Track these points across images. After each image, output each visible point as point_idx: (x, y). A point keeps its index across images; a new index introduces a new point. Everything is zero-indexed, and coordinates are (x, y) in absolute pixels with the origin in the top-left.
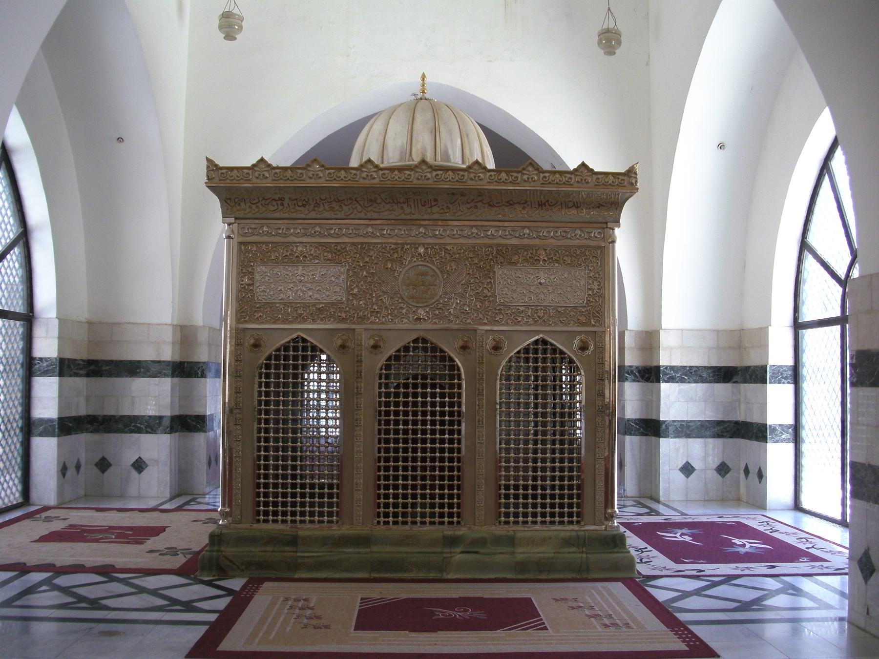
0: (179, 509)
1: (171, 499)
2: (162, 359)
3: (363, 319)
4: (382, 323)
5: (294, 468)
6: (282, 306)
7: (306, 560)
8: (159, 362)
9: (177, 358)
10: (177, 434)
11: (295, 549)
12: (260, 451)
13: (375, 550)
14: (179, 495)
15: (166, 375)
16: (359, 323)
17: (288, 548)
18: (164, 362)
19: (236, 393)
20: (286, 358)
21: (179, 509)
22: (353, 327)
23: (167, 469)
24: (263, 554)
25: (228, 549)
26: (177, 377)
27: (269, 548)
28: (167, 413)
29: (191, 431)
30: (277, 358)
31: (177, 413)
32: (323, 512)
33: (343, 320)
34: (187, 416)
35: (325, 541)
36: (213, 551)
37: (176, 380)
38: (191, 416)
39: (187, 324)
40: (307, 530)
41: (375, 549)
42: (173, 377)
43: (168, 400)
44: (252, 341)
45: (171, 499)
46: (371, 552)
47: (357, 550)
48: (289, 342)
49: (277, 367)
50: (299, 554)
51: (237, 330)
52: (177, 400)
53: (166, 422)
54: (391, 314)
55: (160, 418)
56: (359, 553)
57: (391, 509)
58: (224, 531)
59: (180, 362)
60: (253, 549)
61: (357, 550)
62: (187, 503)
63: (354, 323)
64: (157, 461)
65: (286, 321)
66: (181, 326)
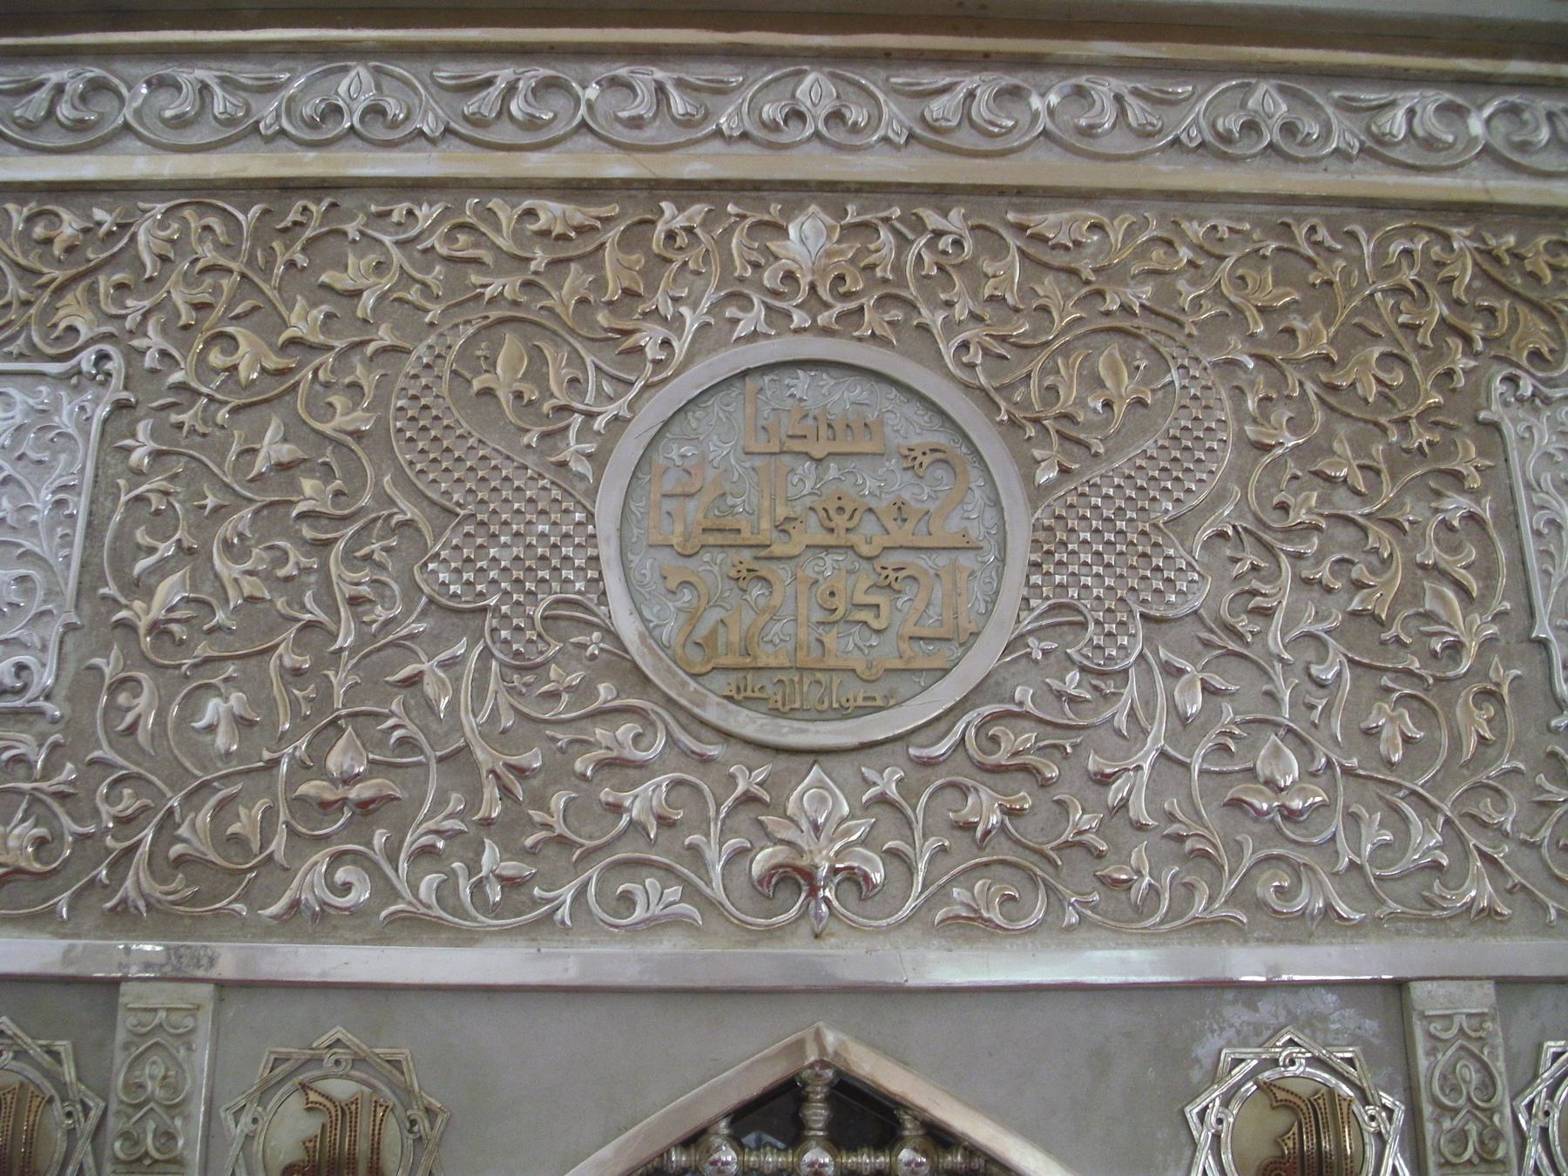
22: (100, 953)
54: (506, 830)
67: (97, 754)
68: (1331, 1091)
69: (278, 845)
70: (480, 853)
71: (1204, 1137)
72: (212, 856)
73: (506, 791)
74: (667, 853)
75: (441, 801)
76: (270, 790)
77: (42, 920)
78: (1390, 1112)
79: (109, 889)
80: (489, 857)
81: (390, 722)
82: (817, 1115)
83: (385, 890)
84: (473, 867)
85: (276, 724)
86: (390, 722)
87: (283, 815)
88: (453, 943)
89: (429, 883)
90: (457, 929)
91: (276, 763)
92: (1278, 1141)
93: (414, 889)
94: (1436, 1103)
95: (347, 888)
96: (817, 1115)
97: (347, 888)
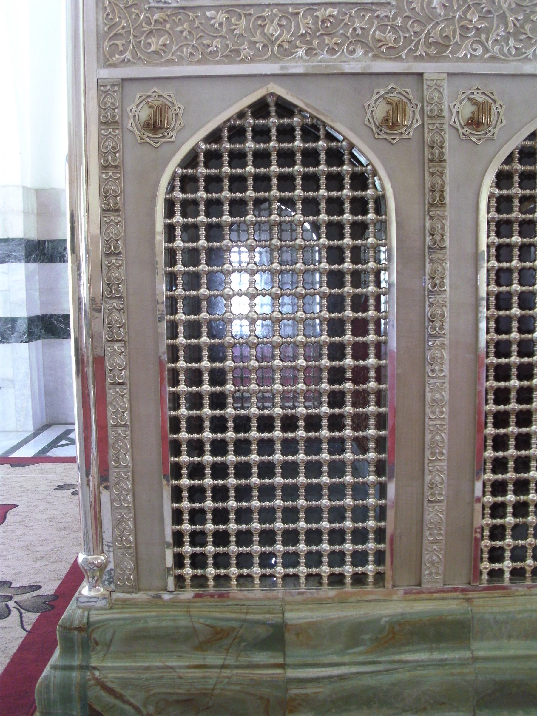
0: (40, 458)
1: (36, 434)
2: (11, 236)
3: (441, 48)
4: (494, 59)
5: (219, 401)
6: (222, 16)
7: (310, 690)
8: (7, 240)
9: (33, 235)
10: (40, 342)
11: (280, 661)
12: (176, 407)
13: (482, 653)
14: (46, 426)
15: (17, 260)
16: (430, 58)
17: (261, 657)
18: (13, 240)
19: (108, 255)
20: (237, 158)
21: (40, 458)
22: (417, 67)
23: (28, 392)
24: (199, 673)
25: (108, 664)
26: (35, 261)
27: (213, 659)
28: (22, 312)
29: (59, 337)
30: (213, 158)
31: (37, 312)
32: (342, 554)
33: (393, 53)
34: (52, 316)
35: (354, 634)
36: (71, 668)
37: (33, 266)
38: (58, 316)
39: (47, 187)
40: (304, 608)
41: (482, 648)
42: (28, 261)
43: (23, 295)
44: (144, 114)
45: (36, 434)
46: (475, 659)
47: (437, 656)
48: (241, 115)
49: (213, 183)
50: (292, 673)
51: (101, 85)
52: (37, 295)
53: (22, 326)
54: (516, 34)
55: (14, 320)
56: (442, 664)
57: (509, 540)
58: (95, 616)
59: (39, 241)
60: (173, 663)
61: (437, 656)
62: (54, 444)
63: (420, 58)
64: (12, 381)
65: (233, 56)
66: (37, 190)
67: (406, 14)
68: (402, 100)
69: (457, 39)
70: (508, 40)
71: (131, 115)
72: (441, 42)
73: (514, 25)
74: (182, 42)
75: (498, 27)
76: (453, 24)
77: (399, 59)
78: (417, 105)
79: (416, 51)
80: (511, 42)
81: (483, 6)
82: (273, 109)
83: (486, 50)
84: (507, 44)
85: (453, 7)
86: (483, 6)
87: (458, 32)
88: (154, 66)
89: (497, 47)
90: (507, 60)
91: (454, 17)
92: (473, 113)
93: (493, 49)
94: (428, 102)
95: (475, 50)
96: (273, 109)
97: (475, 50)
